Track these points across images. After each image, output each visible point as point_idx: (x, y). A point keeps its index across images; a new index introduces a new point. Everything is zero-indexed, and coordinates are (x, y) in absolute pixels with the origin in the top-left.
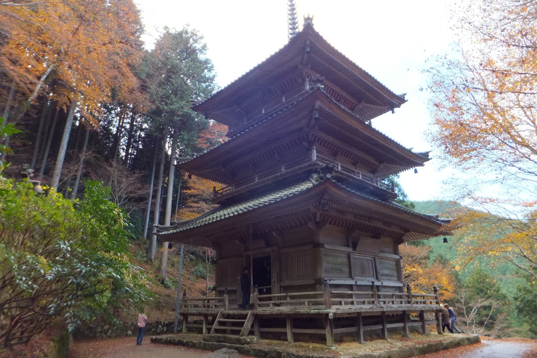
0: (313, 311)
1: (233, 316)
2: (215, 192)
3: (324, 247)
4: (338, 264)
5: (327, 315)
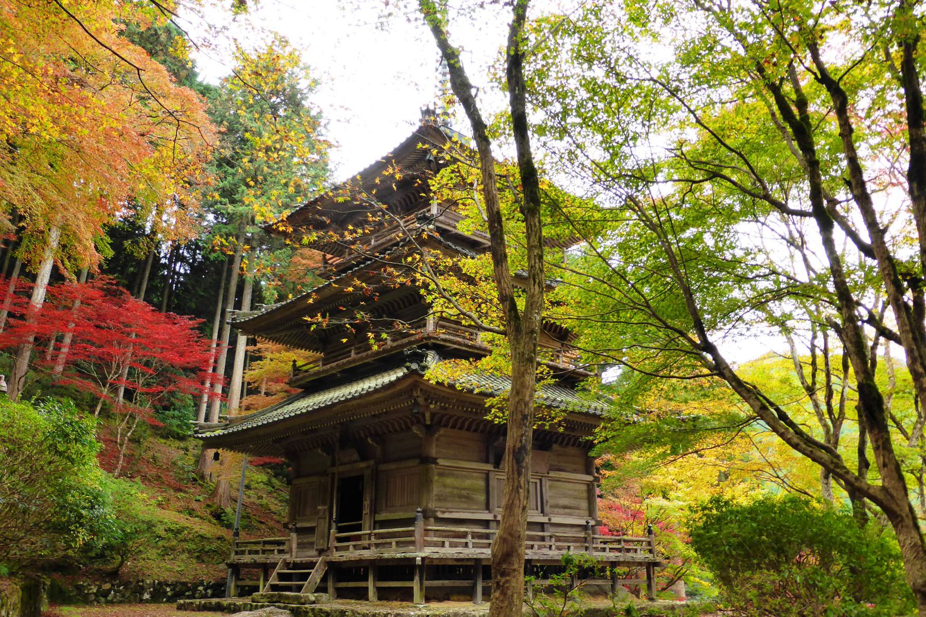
0: (398, 556)
1: (296, 566)
2: (296, 369)
3: (437, 464)
4: (464, 489)
5: (414, 559)
